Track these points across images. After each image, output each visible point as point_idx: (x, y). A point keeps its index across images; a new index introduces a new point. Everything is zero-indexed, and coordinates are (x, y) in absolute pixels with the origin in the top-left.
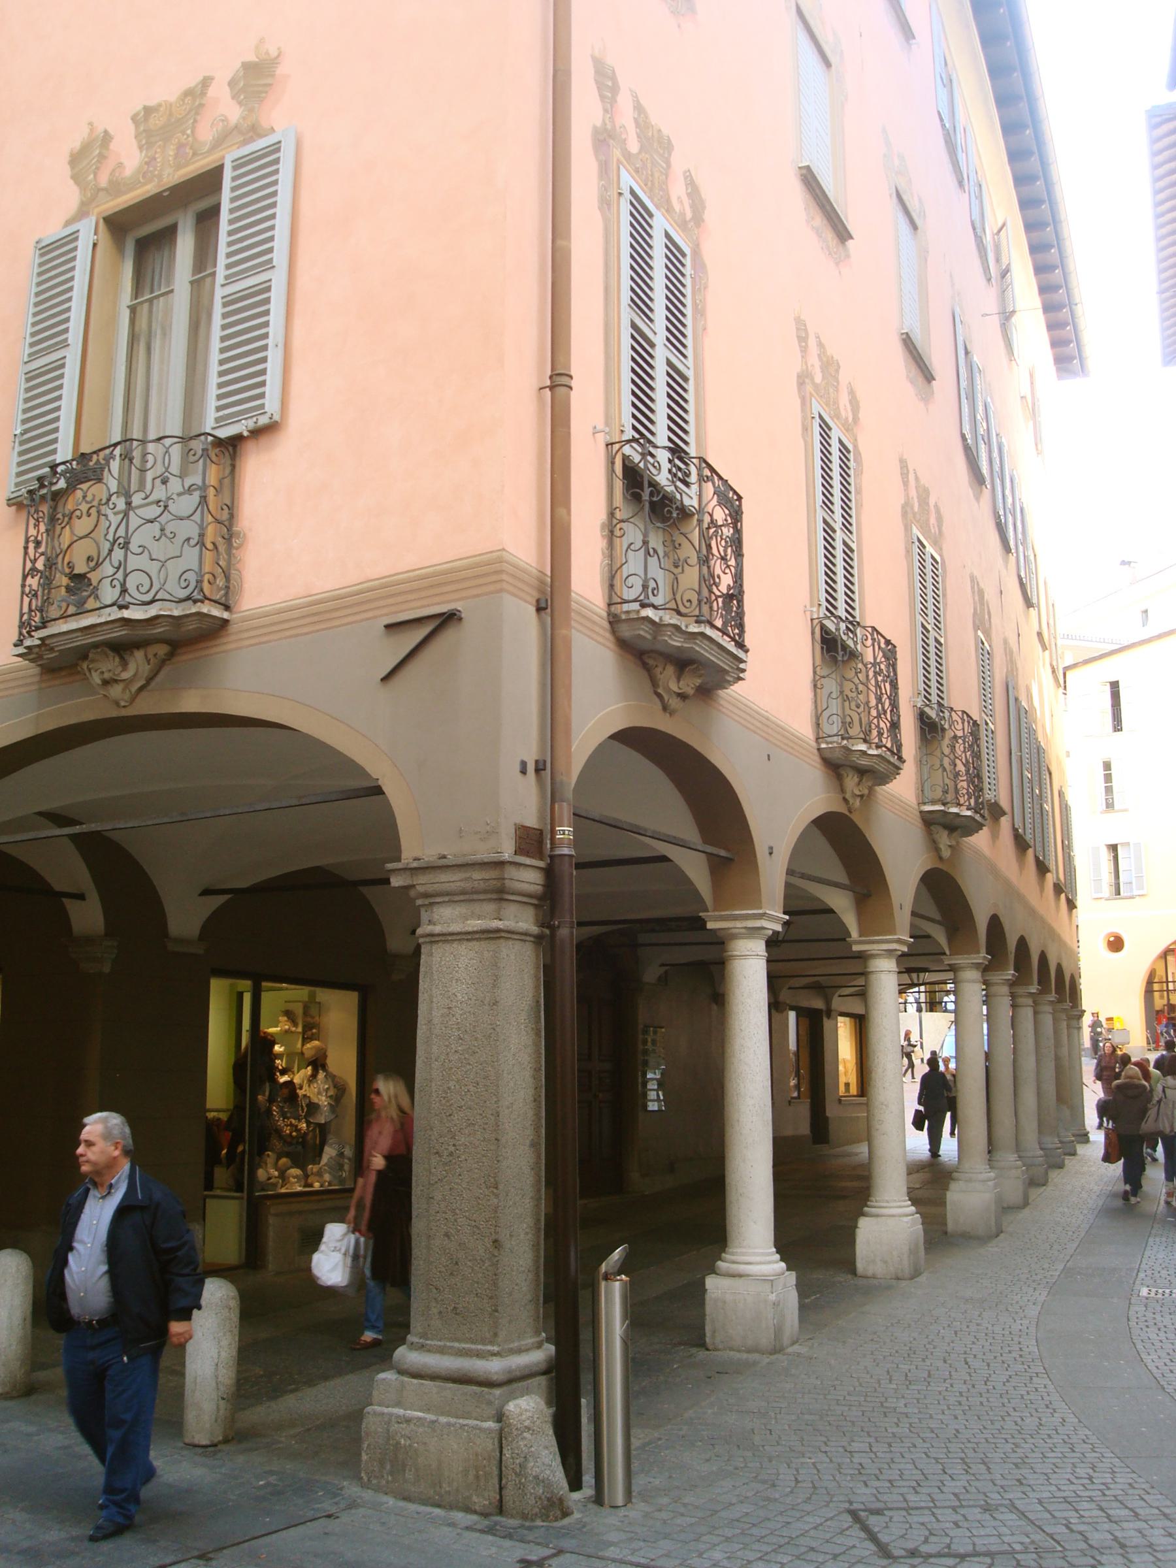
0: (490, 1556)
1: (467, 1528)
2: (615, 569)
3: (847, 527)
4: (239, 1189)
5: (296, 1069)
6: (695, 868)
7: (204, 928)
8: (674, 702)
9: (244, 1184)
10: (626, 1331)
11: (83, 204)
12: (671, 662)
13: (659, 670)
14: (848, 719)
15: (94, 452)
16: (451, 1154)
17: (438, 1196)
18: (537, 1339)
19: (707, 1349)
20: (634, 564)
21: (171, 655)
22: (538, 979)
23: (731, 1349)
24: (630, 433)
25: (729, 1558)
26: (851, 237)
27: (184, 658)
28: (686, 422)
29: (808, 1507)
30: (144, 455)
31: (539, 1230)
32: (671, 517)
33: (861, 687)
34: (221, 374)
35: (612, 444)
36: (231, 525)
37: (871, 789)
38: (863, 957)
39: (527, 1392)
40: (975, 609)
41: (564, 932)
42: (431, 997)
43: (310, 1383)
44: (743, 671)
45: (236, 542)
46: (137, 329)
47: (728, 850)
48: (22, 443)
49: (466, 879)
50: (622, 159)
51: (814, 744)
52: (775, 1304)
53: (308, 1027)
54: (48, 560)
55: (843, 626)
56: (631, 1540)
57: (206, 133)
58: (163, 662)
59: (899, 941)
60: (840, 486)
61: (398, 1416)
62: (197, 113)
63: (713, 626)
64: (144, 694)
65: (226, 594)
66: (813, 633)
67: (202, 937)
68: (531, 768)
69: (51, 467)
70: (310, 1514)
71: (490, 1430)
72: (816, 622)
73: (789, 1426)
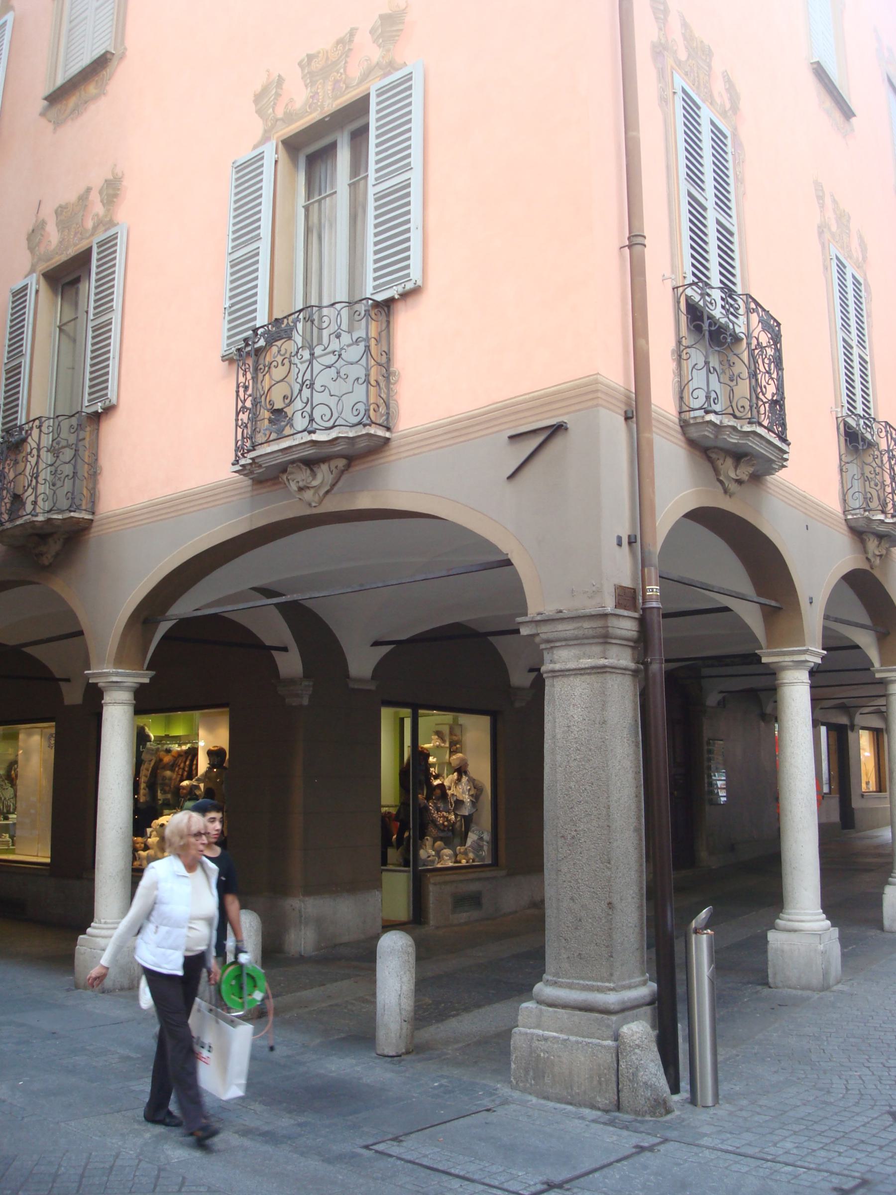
0: (612, 1142)
1: (594, 1121)
2: (683, 384)
3: (861, 344)
4: (406, 864)
6: (750, 615)
7: (376, 670)
8: (733, 487)
9: (409, 861)
11: (265, 131)
13: (721, 461)
14: (869, 496)
15: (285, 317)
16: (573, 837)
17: (565, 869)
18: (643, 978)
19: (770, 987)
20: (698, 379)
21: (348, 466)
22: (636, 704)
23: (790, 988)
24: (690, 279)
25: (797, 1147)
26: (854, 115)
27: (357, 468)
28: (733, 267)
29: (857, 1109)
30: (321, 318)
31: (642, 895)
32: (726, 342)
33: (878, 470)
34: (376, 253)
35: (677, 288)
37: (888, 550)
39: (636, 1018)
41: (655, 667)
42: (554, 719)
43: (467, 1010)
44: (786, 460)
45: (393, 379)
46: (310, 223)
47: (776, 600)
48: (230, 314)
50: (675, 66)
51: (842, 516)
53: (453, 744)
54: (255, 399)
55: (861, 422)
56: (720, 1132)
57: (355, 71)
58: (342, 472)
60: (855, 312)
61: (538, 1036)
62: (347, 56)
63: (760, 425)
64: (329, 496)
65: (387, 419)
66: (838, 428)
67: (374, 677)
68: (625, 541)
69: (254, 331)
70: (474, 1109)
72: (840, 420)
73: (839, 1046)
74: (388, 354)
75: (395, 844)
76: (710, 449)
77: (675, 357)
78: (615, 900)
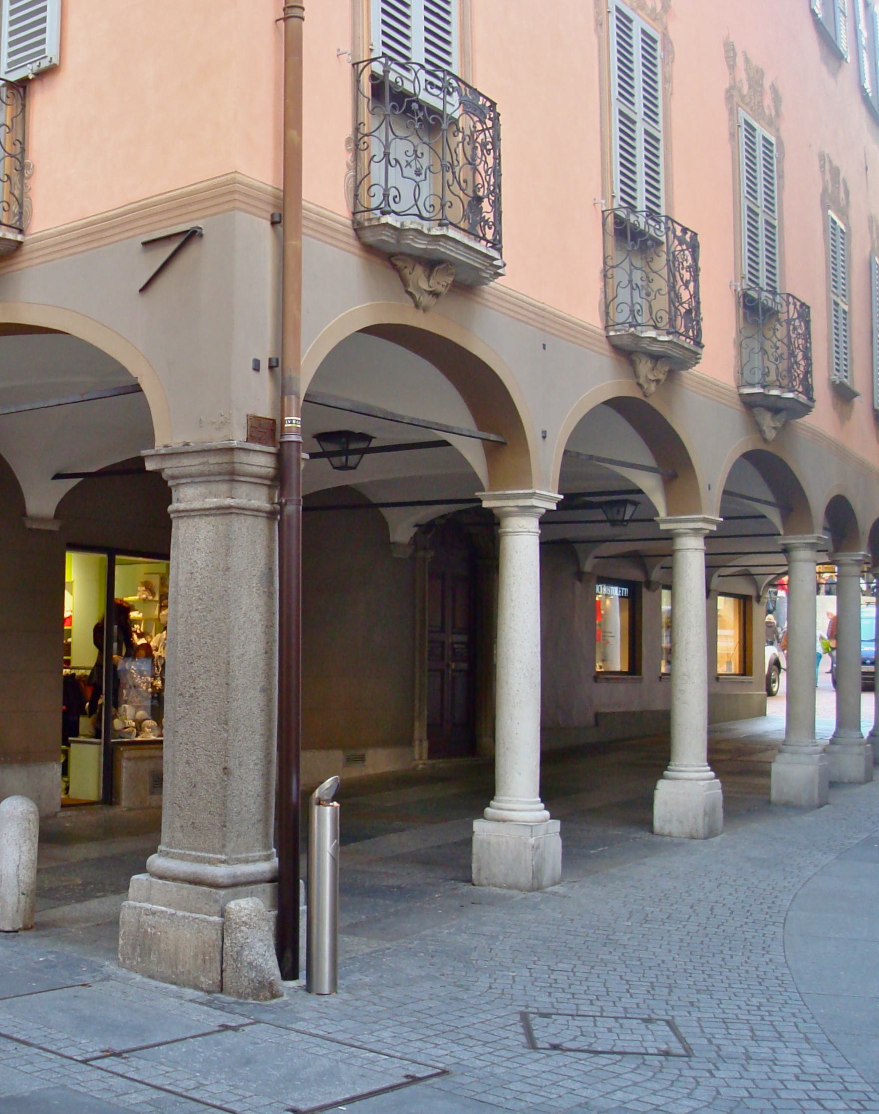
3: (651, 114)
4: (98, 736)
5: (153, 633)
6: (472, 453)
8: (425, 300)
10: (335, 849)
12: (420, 263)
13: (407, 271)
14: (637, 307)
19: (473, 885)
24: (379, 50)
29: (487, 1007)
35: (358, 63)
36: (23, 158)
38: (670, 537)
39: (252, 894)
40: (825, 190)
45: (27, 173)
47: (498, 434)
49: (203, 463)
51: (603, 332)
52: (535, 848)
59: (705, 520)
66: (604, 225)
67: (56, 516)
68: (264, 366)
70: (70, 983)
71: (213, 924)
74: (22, 144)
75: (87, 711)
76: (386, 254)
77: (352, 146)
78: (232, 764)
